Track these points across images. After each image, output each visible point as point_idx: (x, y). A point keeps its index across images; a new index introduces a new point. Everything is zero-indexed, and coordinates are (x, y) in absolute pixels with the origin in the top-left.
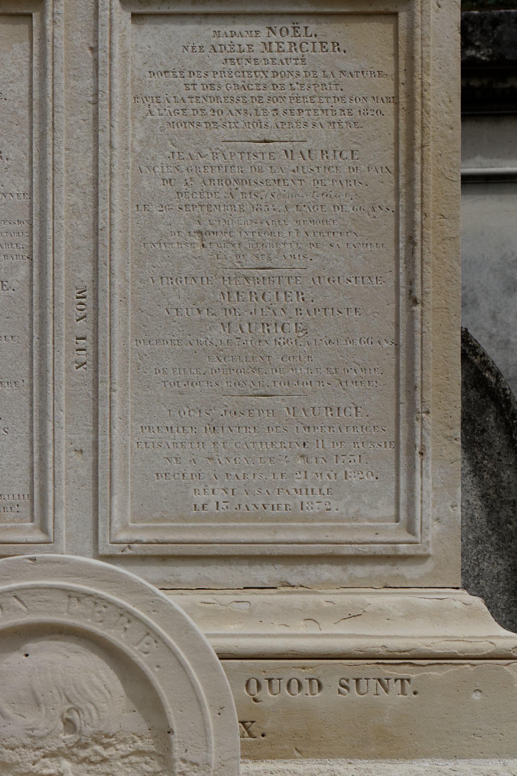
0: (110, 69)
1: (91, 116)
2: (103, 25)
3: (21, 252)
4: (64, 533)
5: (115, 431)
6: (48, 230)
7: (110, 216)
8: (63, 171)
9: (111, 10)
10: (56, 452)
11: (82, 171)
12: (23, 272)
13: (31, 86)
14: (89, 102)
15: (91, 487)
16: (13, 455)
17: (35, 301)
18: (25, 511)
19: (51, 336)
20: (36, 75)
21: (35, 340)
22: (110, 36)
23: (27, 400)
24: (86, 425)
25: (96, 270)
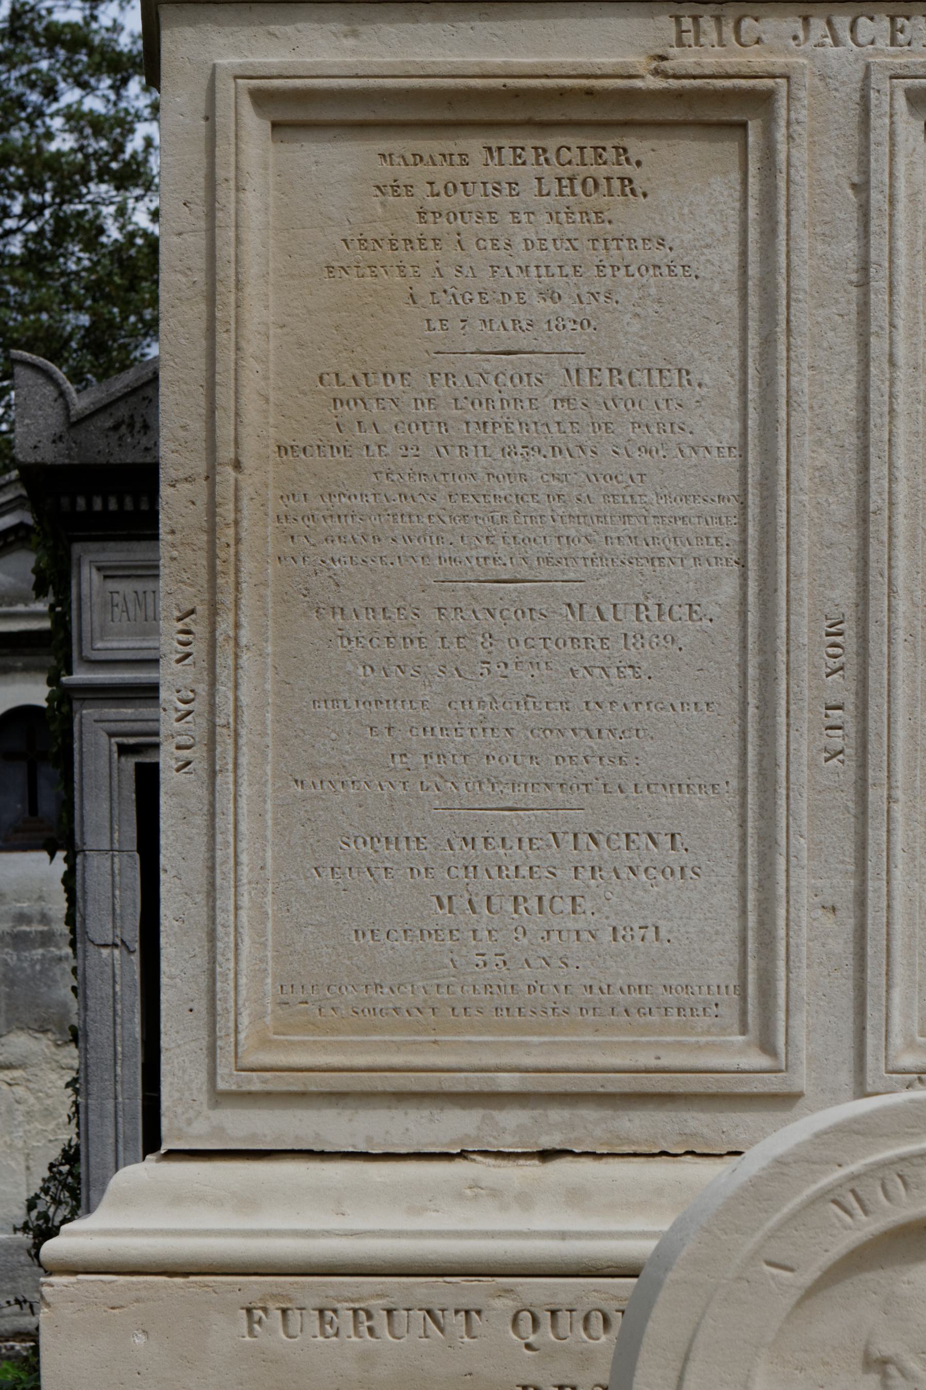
0: (891, 224)
1: (854, 307)
2: (879, 144)
3: (724, 552)
4: (803, 1055)
5: (898, 873)
6: (779, 513)
7: (890, 487)
8: (806, 406)
9: (891, 116)
10: (792, 910)
11: (837, 407)
12: (729, 588)
13: (744, 254)
14: (851, 282)
15: (851, 973)
16: (709, 915)
17: (751, 640)
18: (730, 1013)
19: (783, 703)
20: (753, 234)
21: (751, 710)
22: (891, 164)
23: (735, 817)
24: (843, 862)
25: (863, 585)
